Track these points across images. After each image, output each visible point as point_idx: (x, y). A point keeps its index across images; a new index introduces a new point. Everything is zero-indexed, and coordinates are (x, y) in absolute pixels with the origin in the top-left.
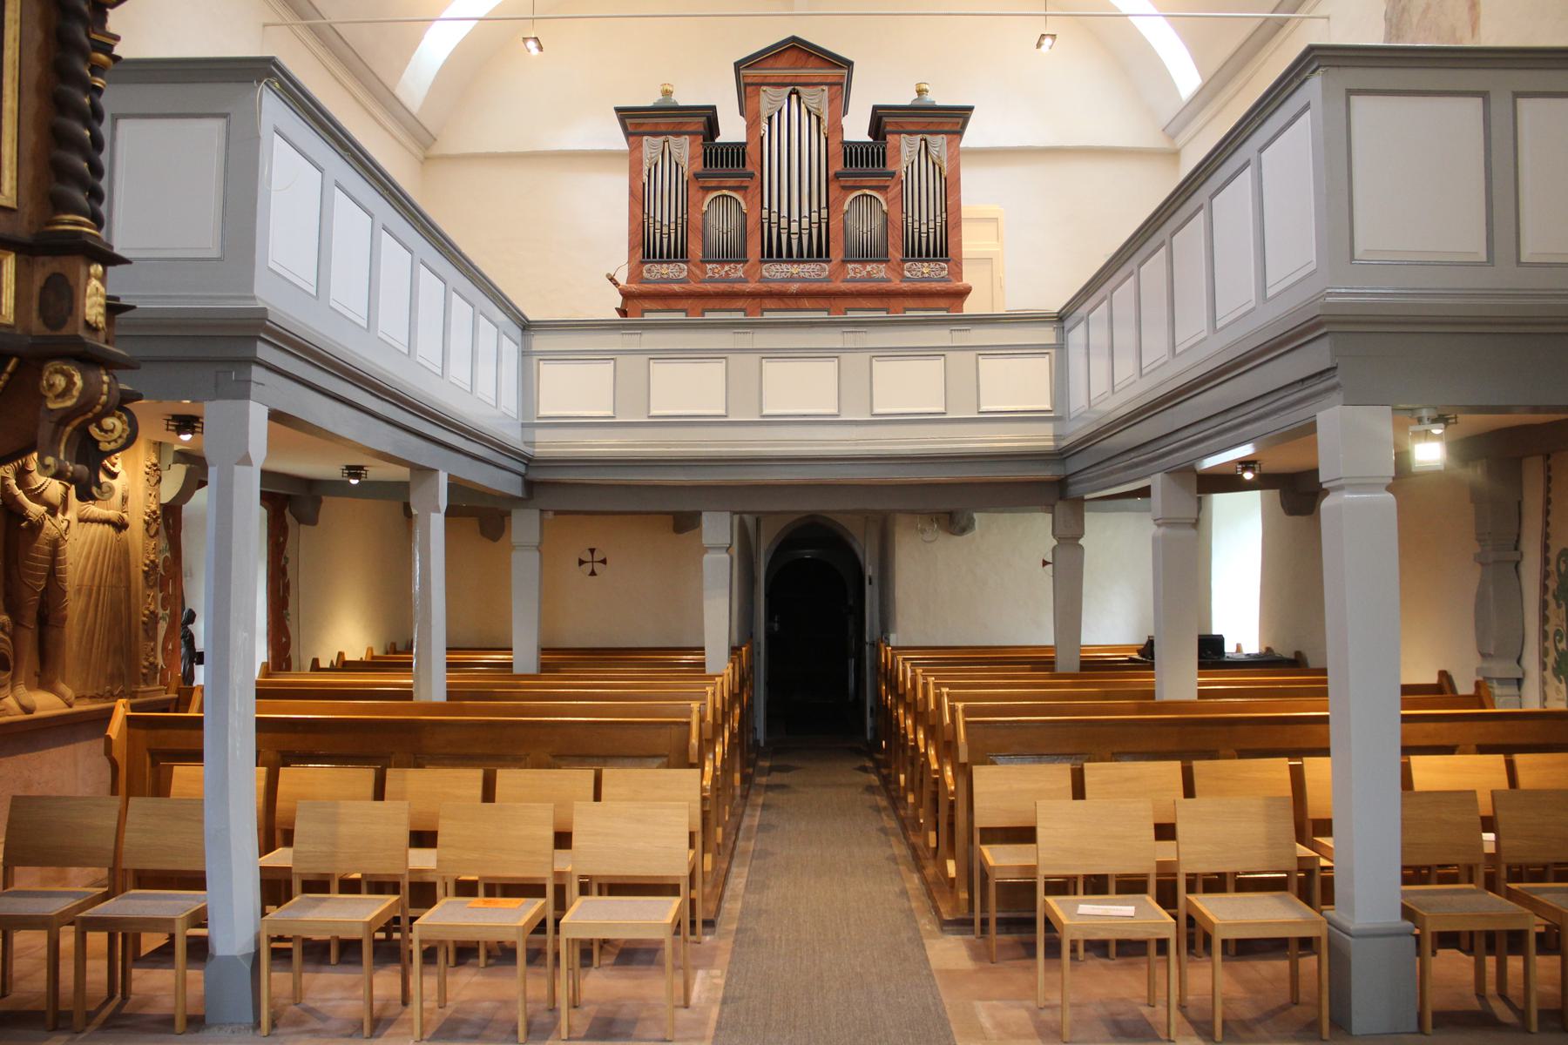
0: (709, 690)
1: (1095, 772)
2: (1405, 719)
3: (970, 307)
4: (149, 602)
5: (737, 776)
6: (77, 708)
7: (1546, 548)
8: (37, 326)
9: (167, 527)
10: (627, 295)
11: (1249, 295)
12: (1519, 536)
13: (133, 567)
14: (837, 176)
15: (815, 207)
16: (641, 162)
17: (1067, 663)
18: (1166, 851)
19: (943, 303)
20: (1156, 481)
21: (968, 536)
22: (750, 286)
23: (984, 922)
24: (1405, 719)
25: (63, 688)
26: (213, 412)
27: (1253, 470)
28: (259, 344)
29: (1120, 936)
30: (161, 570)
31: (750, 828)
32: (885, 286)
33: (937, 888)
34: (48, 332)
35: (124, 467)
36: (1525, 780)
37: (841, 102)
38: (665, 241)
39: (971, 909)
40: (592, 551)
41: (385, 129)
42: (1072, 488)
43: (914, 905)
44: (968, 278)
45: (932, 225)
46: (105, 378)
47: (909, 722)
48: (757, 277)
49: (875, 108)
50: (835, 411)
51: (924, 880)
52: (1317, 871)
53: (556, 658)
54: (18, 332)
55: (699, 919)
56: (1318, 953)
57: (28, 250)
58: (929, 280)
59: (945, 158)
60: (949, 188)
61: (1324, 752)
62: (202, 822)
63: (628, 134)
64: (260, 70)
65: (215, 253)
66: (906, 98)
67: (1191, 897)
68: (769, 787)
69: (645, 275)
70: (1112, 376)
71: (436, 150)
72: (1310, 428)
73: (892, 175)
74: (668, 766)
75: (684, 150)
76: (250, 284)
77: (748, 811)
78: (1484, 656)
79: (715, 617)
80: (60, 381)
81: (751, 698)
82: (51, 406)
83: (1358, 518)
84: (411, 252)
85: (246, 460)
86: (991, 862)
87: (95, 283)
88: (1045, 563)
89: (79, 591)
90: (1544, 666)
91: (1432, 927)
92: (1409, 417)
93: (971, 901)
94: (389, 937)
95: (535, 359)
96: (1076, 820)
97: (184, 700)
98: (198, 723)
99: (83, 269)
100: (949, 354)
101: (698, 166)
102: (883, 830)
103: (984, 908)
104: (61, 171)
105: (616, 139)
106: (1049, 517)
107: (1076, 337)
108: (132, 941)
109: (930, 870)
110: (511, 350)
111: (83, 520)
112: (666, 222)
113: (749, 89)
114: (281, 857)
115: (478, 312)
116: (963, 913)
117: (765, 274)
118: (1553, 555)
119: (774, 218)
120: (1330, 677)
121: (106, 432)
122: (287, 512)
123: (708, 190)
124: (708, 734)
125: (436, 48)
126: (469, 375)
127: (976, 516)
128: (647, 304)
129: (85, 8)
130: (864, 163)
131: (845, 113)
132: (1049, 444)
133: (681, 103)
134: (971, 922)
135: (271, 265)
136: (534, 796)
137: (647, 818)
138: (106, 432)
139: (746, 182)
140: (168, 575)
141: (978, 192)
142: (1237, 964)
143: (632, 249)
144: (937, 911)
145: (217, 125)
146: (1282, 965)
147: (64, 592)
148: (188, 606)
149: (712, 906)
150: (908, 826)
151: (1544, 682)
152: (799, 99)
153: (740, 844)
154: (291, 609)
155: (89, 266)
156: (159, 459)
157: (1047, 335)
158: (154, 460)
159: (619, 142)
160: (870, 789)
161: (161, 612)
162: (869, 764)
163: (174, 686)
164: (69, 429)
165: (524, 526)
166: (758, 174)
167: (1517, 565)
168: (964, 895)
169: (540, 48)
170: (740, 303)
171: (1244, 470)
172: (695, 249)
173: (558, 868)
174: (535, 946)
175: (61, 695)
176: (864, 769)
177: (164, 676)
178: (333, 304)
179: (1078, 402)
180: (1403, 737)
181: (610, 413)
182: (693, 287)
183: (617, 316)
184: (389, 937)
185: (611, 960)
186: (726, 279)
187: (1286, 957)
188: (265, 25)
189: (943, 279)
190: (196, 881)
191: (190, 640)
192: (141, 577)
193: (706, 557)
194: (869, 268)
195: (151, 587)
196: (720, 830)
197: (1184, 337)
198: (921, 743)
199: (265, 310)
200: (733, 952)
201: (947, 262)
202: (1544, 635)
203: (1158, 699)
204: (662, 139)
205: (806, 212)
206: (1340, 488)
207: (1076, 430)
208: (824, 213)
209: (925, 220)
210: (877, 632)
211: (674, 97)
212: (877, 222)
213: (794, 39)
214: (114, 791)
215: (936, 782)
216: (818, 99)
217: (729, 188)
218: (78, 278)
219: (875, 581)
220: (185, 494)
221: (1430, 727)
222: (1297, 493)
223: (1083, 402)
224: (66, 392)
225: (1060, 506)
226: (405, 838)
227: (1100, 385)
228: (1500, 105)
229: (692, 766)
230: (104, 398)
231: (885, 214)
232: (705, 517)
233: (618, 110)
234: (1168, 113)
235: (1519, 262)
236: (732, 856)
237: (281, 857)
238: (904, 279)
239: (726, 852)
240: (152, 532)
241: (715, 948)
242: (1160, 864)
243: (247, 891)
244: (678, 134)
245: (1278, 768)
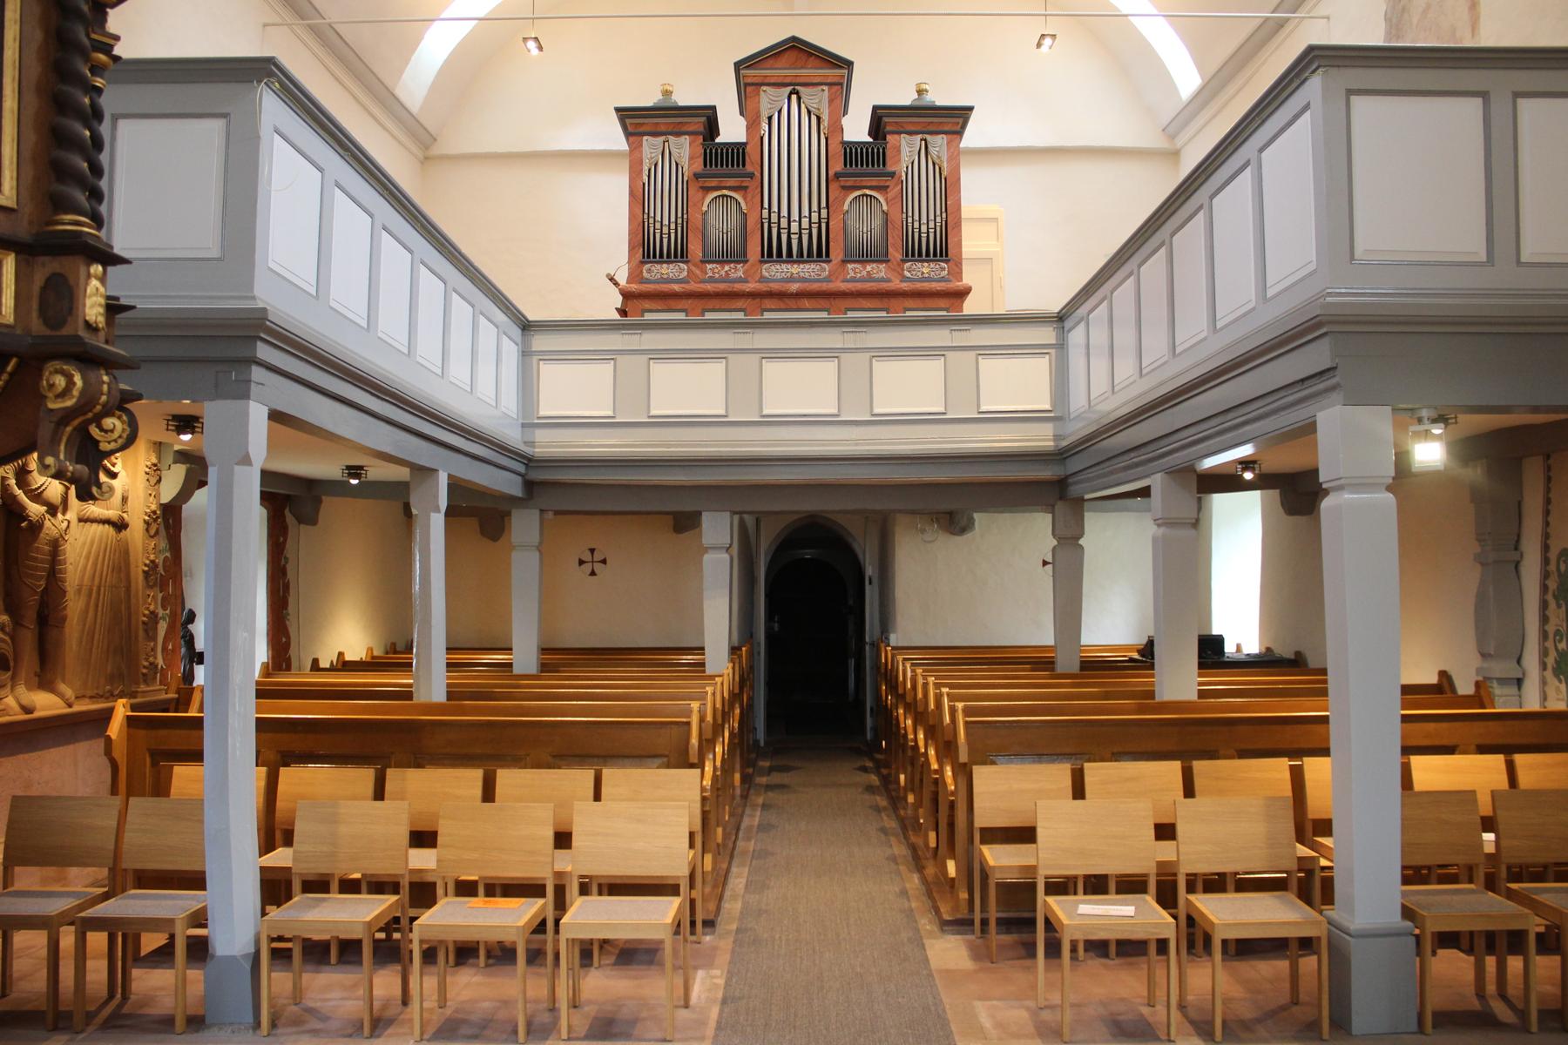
0: (709, 690)
1: (1095, 772)
2: (1405, 719)
3: (970, 307)
4: (149, 602)
5: (737, 776)
6: (77, 708)
7: (1546, 548)
8: (37, 326)
9: (167, 527)
10: (627, 295)
11: (1249, 295)
12: (1519, 536)
14: (837, 176)
15: (815, 207)
16: (641, 162)
17: (1067, 663)
18: (1166, 851)
19: (942, 303)
20: (1156, 481)
21: (968, 536)
22: (750, 286)
23: (985, 922)
24: (1405, 719)
26: (213, 412)
27: (1253, 470)
28: (259, 344)
30: (161, 569)
31: (750, 828)
33: (937, 888)
34: (48, 332)
35: (124, 467)
36: (1525, 780)
37: (841, 102)
38: (665, 241)
39: (971, 909)
40: (592, 551)
41: (385, 129)
42: (1072, 488)
44: (968, 278)
45: (932, 225)
46: (105, 378)
47: (909, 722)
48: (757, 277)
49: (875, 108)
50: (835, 411)
51: (924, 880)
53: (556, 658)
54: (19, 332)
55: (699, 919)
56: (1318, 953)
57: (26, 251)
58: (929, 280)
59: (945, 158)
60: (949, 188)
61: (1324, 752)
62: (202, 822)
64: (260, 70)
65: (215, 253)
66: (906, 98)
67: (1192, 897)
68: (769, 787)
69: (645, 275)
70: (1111, 376)
71: (436, 150)
72: (1310, 428)
73: (892, 175)
74: (668, 766)
75: (684, 150)
76: (251, 288)
77: (748, 811)
78: (1484, 656)
79: (715, 617)
80: (60, 381)
81: (750, 699)
82: (51, 406)
83: (1358, 518)
85: (246, 460)
86: (991, 862)
87: (94, 283)
88: (1045, 563)
89: (79, 591)
90: (1544, 666)
91: (1433, 927)
92: (1409, 417)
93: (971, 901)
95: (535, 359)
96: (1076, 820)
97: (184, 700)
98: (198, 723)
99: (83, 269)
100: (949, 354)
101: (698, 166)
102: (884, 831)
103: (984, 908)
104: (61, 172)
105: (616, 139)
106: (1049, 517)
107: (1076, 336)
108: (132, 941)
109: (930, 870)
110: (511, 350)
111: (83, 520)
112: (666, 222)
113: (749, 89)
114: (281, 857)
115: (477, 312)
116: (963, 913)
117: (765, 274)
118: (1553, 555)
119: (774, 218)
120: (1330, 677)
121: (106, 431)
122: (287, 512)
123: (707, 190)
125: (436, 48)
126: (469, 375)
127: (976, 516)
128: (647, 305)
130: (864, 163)
131: (845, 113)
132: (1049, 444)
133: (681, 103)
134: (971, 922)
135: (271, 265)
136: (534, 796)
137: (647, 818)
138: (106, 431)
139: (746, 182)
140: (169, 574)
141: (978, 193)
143: (632, 249)
144: (937, 911)
145: (217, 125)
146: (1282, 965)
147: (64, 592)
148: (188, 606)
149: (712, 906)
150: (908, 826)
151: (1544, 682)
152: (799, 99)
153: (740, 844)
155: (89, 266)
156: (159, 459)
157: (1047, 335)
158: (154, 460)
159: (620, 142)
160: (870, 789)
161: (161, 612)
162: (869, 764)
163: (174, 687)
164: (69, 429)
165: (524, 526)
166: (758, 174)
167: (1517, 565)
168: (964, 895)
169: (540, 48)
170: (740, 303)
171: (1244, 470)
172: (695, 249)
173: (558, 868)
174: (535, 946)
175: (61, 696)
176: (864, 769)
178: (333, 304)
179: (1078, 402)
181: (610, 413)
182: (693, 286)
183: (617, 316)
185: (612, 959)
186: (726, 279)
187: (1286, 957)
188: (265, 25)
189: (943, 279)
190: (196, 881)
191: (190, 640)
192: (141, 577)
193: (706, 557)
194: (869, 268)
195: (151, 587)
196: (720, 830)
197: (1184, 337)
198: (921, 743)
199: (265, 310)
200: (733, 951)
201: (947, 262)
202: (1544, 635)
203: (1158, 699)
204: (662, 139)
205: (806, 212)
206: (1340, 488)
207: (1076, 430)
208: (824, 213)
209: (925, 220)
211: (674, 97)
212: (877, 222)
213: (794, 39)
214: (114, 791)
215: (936, 781)
216: (818, 99)
217: (730, 188)
218: (78, 278)
219: (875, 581)
220: (185, 494)
221: (1431, 726)
222: (1297, 493)
225: (1060, 506)
226: (405, 838)
227: (1100, 385)
229: (692, 766)
230: (104, 398)
231: (885, 214)
232: (706, 518)
233: (618, 110)
234: (1168, 113)
235: (1518, 262)
236: (732, 857)
237: (281, 857)
238: (904, 279)
239: (726, 852)
240: (152, 532)
241: (715, 948)
242: (1160, 864)
243: (247, 891)
244: (678, 134)
245: (1279, 768)
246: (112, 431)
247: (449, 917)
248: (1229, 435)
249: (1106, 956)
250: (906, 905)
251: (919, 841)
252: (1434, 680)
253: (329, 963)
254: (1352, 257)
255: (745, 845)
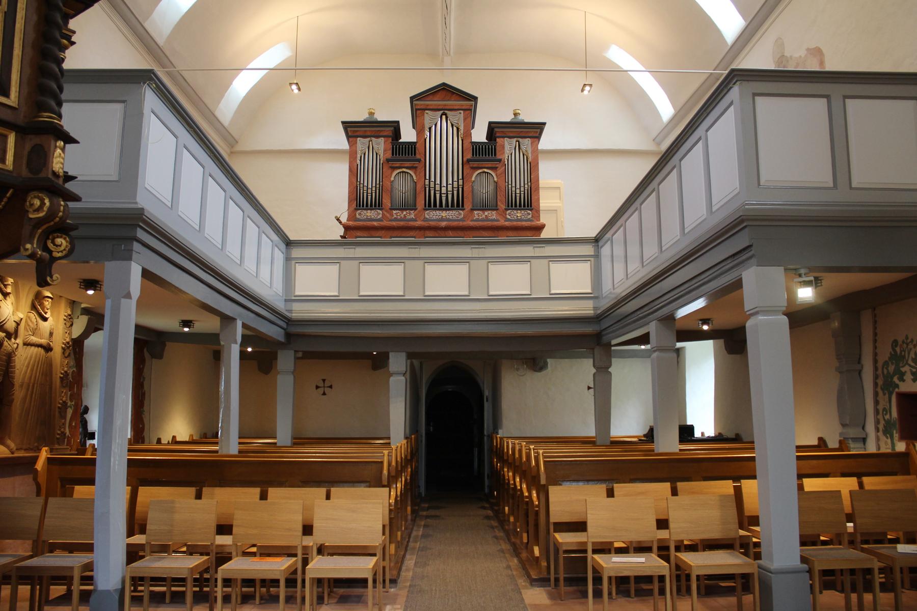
1: (618, 488)
2: (798, 458)
3: (544, 234)
4: (62, 395)
5: (409, 508)
6: (16, 455)
7: (875, 361)
8: (25, 172)
9: (75, 353)
10: (347, 228)
11: (703, 211)
12: (860, 356)
13: (54, 375)
14: (469, 161)
15: (455, 179)
16: (356, 153)
18: (663, 534)
20: (652, 328)
21: (543, 372)
22: (419, 223)
23: (557, 580)
24: (798, 458)
25: (9, 442)
26: (110, 270)
27: (708, 324)
29: (636, 574)
31: (417, 536)
32: (496, 223)
33: (527, 564)
34: (32, 176)
35: (52, 315)
36: (867, 487)
37: (471, 122)
39: (549, 573)
40: (324, 380)
42: (604, 338)
43: (515, 573)
44: (543, 220)
45: (522, 189)
46: (62, 203)
47: (511, 474)
48: (422, 218)
49: (490, 123)
51: (521, 561)
52: (751, 545)
53: (299, 440)
54: (15, 175)
56: (753, 593)
57: (22, 131)
58: (521, 220)
59: (530, 152)
60: (532, 169)
61: (754, 477)
62: (92, 512)
63: (348, 137)
65: (115, 177)
66: (508, 118)
67: (678, 554)
68: (427, 517)
69: (358, 216)
71: (238, 148)
72: (738, 285)
73: (500, 160)
74: (370, 487)
75: (381, 145)
76: (135, 196)
77: (415, 528)
78: (844, 425)
79: (395, 417)
80: (37, 202)
82: (31, 216)
83: (769, 338)
84: (225, 191)
85: (128, 296)
86: (560, 540)
87: (59, 151)
88: (589, 388)
89: (21, 386)
90: (877, 430)
91: (818, 567)
92: (794, 273)
93: (548, 567)
94: (201, 589)
95: (293, 262)
96: (612, 515)
97: (82, 449)
98: (93, 462)
99: (53, 142)
101: (389, 155)
102: (496, 537)
103: (556, 572)
104: (43, 90)
105: (342, 142)
107: (606, 250)
108: (45, 592)
109: (524, 555)
110: (279, 256)
111: (26, 344)
114: (139, 539)
116: (544, 574)
117: (427, 216)
118: (880, 365)
119: (432, 185)
121: (57, 246)
122: (145, 350)
123: (394, 168)
124: (393, 474)
125: (242, 85)
126: (258, 268)
127: (548, 360)
129: (61, 4)
130: (484, 155)
131: (473, 127)
133: (379, 119)
134: (549, 580)
135: (146, 186)
136: (288, 506)
137: (358, 516)
138: (57, 246)
139: (416, 164)
140: (75, 381)
141: (548, 173)
142: (706, 599)
144: (529, 576)
145: (119, 107)
146: (733, 600)
147: (13, 385)
148: (84, 404)
149: (395, 572)
150: (510, 535)
151: (878, 439)
153: (411, 544)
154: (145, 408)
155: (56, 141)
157: (588, 250)
158: (69, 312)
159: (344, 144)
160: (488, 517)
161: (69, 403)
162: (487, 505)
163: (75, 447)
164: (40, 231)
165: (286, 361)
166: (423, 160)
167: (860, 372)
168: (544, 564)
169: (299, 89)
170: (412, 233)
171: (703, 324)
172: (387, 202)
174: (289, 594)
175: (8, 447)
176: (484, 508)
177: (69, 443)
178: (180, 213)
179: (607, 287)
180: (798, 468)
181: (336, 294)
182: (385, 223)
184: (201, 589)
185: (335, 600)
186: (404, 219)
187: (735, 596)
189: (529, 220)
190: (89, 548)
191: (85, 424)
192: (58, 381)
193: (392, 379)
194: (486, 213)
195: (64, 387)
196: (399, 533)
198: (518, 484)
199: (143, 209)
201: (531, 210)
202: (877, 412)
204: (368, 139)
205: (450, 181)
206: (757, 313)
207: (605, 304)
208: (461, 182)
209: (517, 184)
210: (491, 428)
211: (375, 116)
212: (491, 188)
213: (444, 84)
214: (38, 494)
216: (458, 117)
217: (407, 168)
220: (86, 334)
221: (814, 462)
222: (733, 342)
223: (610, 286)
224: (38, 210)
225: (597, 350)
226: (213, 529)
227: (619, 274)
228: (837, 103)
229: (384, 486)
230: (61, 214)
231: (496, 183)
232: (391, 355)
233: (343, 123)
235: (851, 188)
237: (139, 539)
239: (403, 547)
240: (66, 355)
241: (396, 595)
242: (659, 540)
243: (118, 554)
244: (377, 137)
245: (726, 487)
246: (60, 246)
247: (238, 566)
248: (694, 293)
249: (629, 596)
250: (510, 572)
251: (518, 541)
252: (815, 442)
253: (164, 602)
254: (759, 184)
255: (414, 545)
